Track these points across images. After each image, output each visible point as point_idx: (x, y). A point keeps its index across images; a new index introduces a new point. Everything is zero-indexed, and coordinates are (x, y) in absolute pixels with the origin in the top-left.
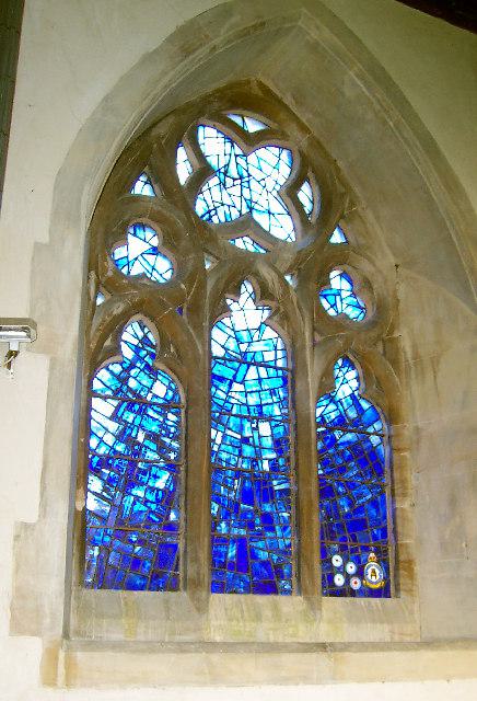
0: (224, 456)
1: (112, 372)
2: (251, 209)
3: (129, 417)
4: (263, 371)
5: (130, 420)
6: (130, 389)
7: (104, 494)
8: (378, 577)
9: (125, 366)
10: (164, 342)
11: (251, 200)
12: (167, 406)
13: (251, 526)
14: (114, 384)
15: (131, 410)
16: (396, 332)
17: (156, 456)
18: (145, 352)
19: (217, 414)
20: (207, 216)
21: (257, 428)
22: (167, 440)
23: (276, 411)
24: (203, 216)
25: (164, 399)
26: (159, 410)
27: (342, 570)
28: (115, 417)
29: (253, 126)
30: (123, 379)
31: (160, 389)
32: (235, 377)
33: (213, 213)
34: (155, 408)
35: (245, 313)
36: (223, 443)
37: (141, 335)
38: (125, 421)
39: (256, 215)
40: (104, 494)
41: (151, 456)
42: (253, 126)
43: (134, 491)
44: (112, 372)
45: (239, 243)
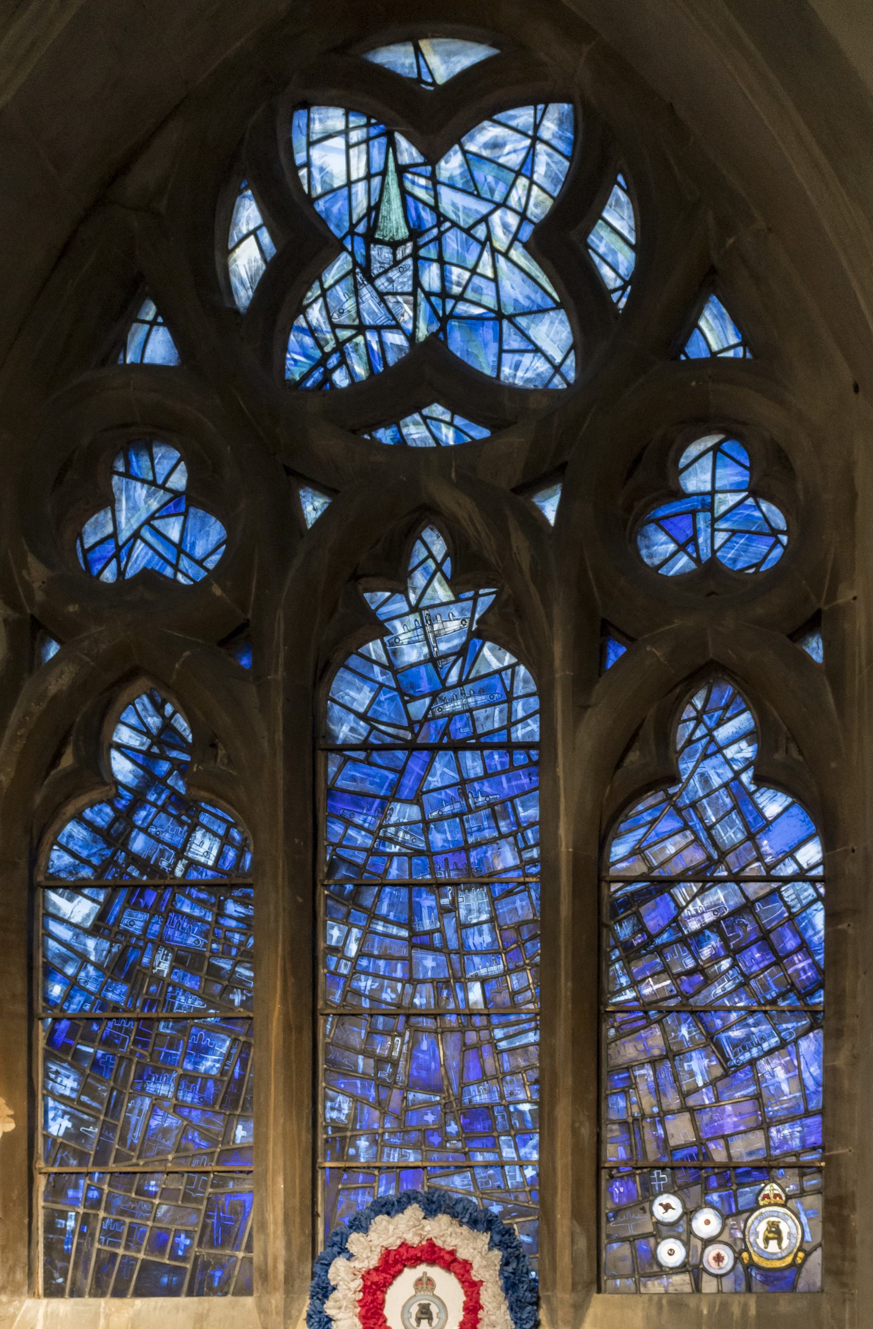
0: (366, 984)
1: (90, 825)
2: (444, 320)
3: (136, 922)
4: (473, 764)
5: (137, 927)
6: (134, 859)
7: (84, 1098)
8: (785, 1243)
9: (122, 804)
10: (207, 743)
11: (444, 294)
12: (222, 884)
13: (423, 1139)
14: (96, 853)
15: (136, 907)
16: (842, 587)
17: (198, 1004)
18: (165, 766)
19: (349, 887)
20: (317, 375)
21: (454, 907)
22: (225, 965)
23: (506, 858)
24: (306, 377)
25: (215, 868)
26: (203, 896)
27: (682, 1229)
28: (99, 926)
29: (445, 61)
30: (114, 837)
31: (204, 848)
32: (395, 787)
33: (333, 361)
34: (194, 892)
35: (427, 617)
36: (360, 954)
37: (154, 722)
38: (126, 933)
39: (458, 341)
40: (84, 1098)
41: (186, 1003)
42: (445, 61)
43: (151, 1087)
44: (90, 825)
45: (415, 432)
